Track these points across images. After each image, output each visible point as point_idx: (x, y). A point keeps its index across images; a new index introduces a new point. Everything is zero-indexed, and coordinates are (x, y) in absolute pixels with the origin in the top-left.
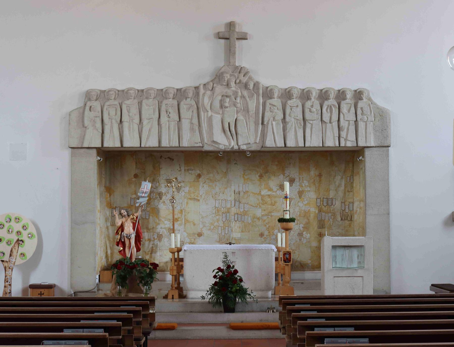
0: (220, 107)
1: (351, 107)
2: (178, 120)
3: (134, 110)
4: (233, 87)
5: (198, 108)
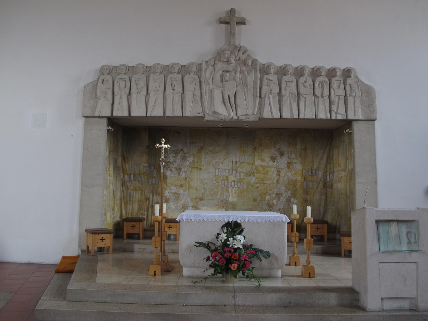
0: (221, 81)
1: (340, 83)
2: (182, 92)
3: (142, 83)
4: (233, 63)
5: (200, 82)
